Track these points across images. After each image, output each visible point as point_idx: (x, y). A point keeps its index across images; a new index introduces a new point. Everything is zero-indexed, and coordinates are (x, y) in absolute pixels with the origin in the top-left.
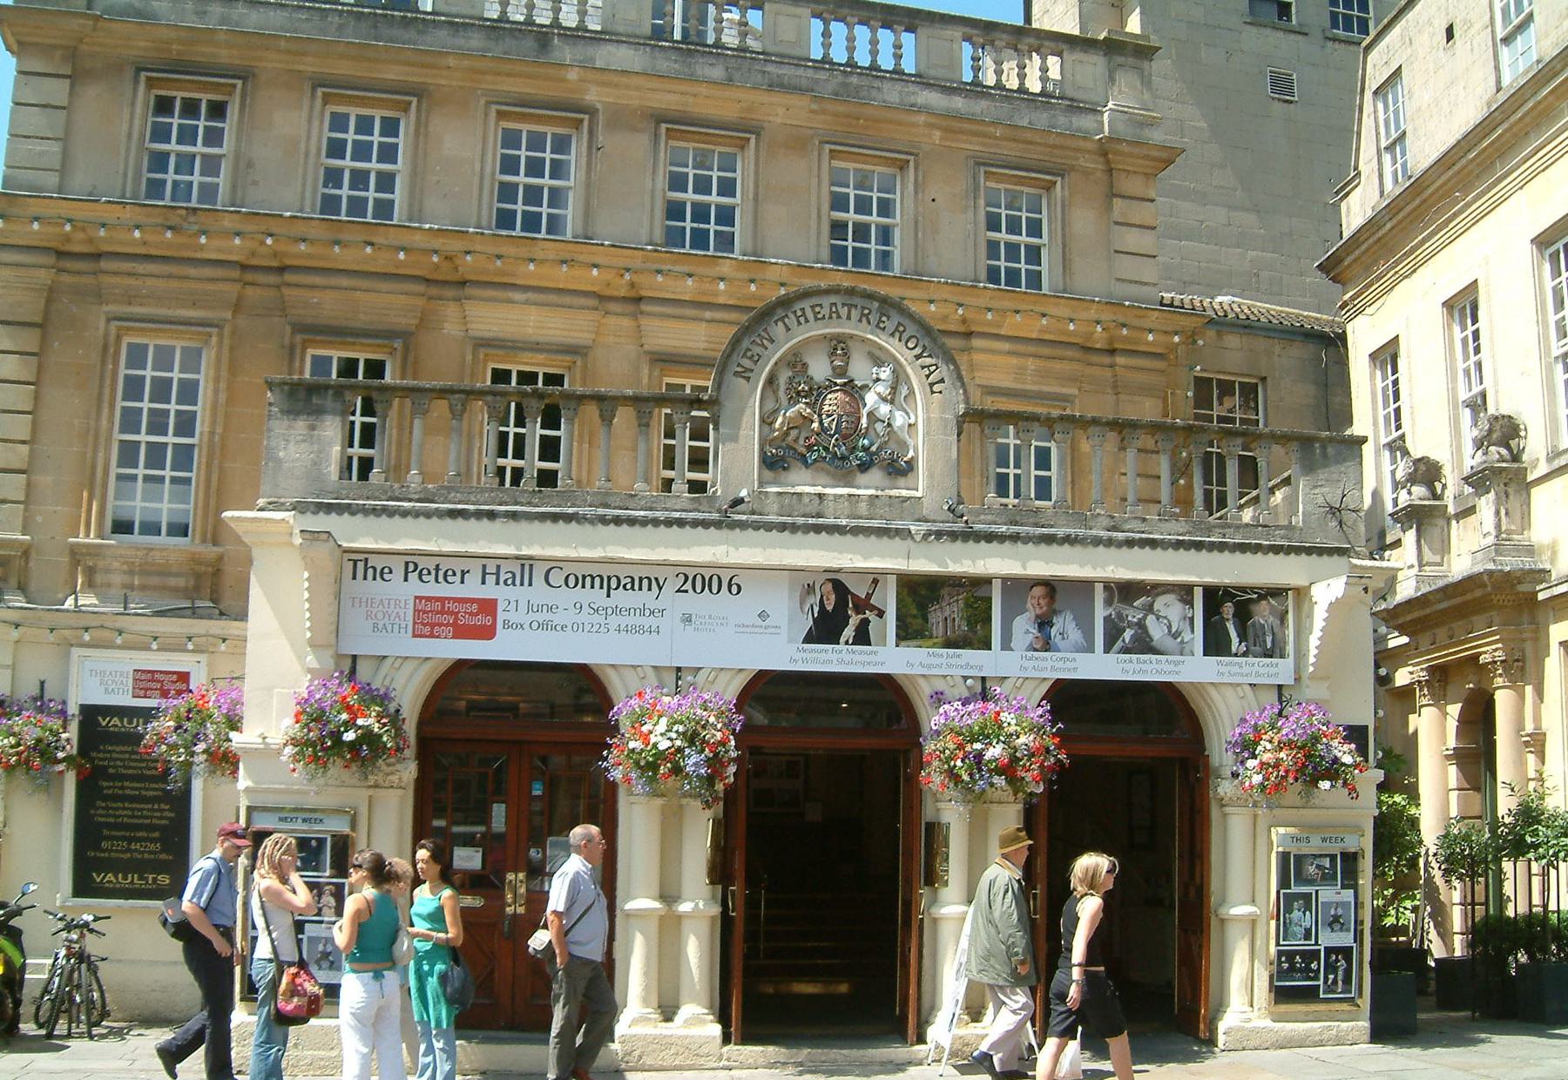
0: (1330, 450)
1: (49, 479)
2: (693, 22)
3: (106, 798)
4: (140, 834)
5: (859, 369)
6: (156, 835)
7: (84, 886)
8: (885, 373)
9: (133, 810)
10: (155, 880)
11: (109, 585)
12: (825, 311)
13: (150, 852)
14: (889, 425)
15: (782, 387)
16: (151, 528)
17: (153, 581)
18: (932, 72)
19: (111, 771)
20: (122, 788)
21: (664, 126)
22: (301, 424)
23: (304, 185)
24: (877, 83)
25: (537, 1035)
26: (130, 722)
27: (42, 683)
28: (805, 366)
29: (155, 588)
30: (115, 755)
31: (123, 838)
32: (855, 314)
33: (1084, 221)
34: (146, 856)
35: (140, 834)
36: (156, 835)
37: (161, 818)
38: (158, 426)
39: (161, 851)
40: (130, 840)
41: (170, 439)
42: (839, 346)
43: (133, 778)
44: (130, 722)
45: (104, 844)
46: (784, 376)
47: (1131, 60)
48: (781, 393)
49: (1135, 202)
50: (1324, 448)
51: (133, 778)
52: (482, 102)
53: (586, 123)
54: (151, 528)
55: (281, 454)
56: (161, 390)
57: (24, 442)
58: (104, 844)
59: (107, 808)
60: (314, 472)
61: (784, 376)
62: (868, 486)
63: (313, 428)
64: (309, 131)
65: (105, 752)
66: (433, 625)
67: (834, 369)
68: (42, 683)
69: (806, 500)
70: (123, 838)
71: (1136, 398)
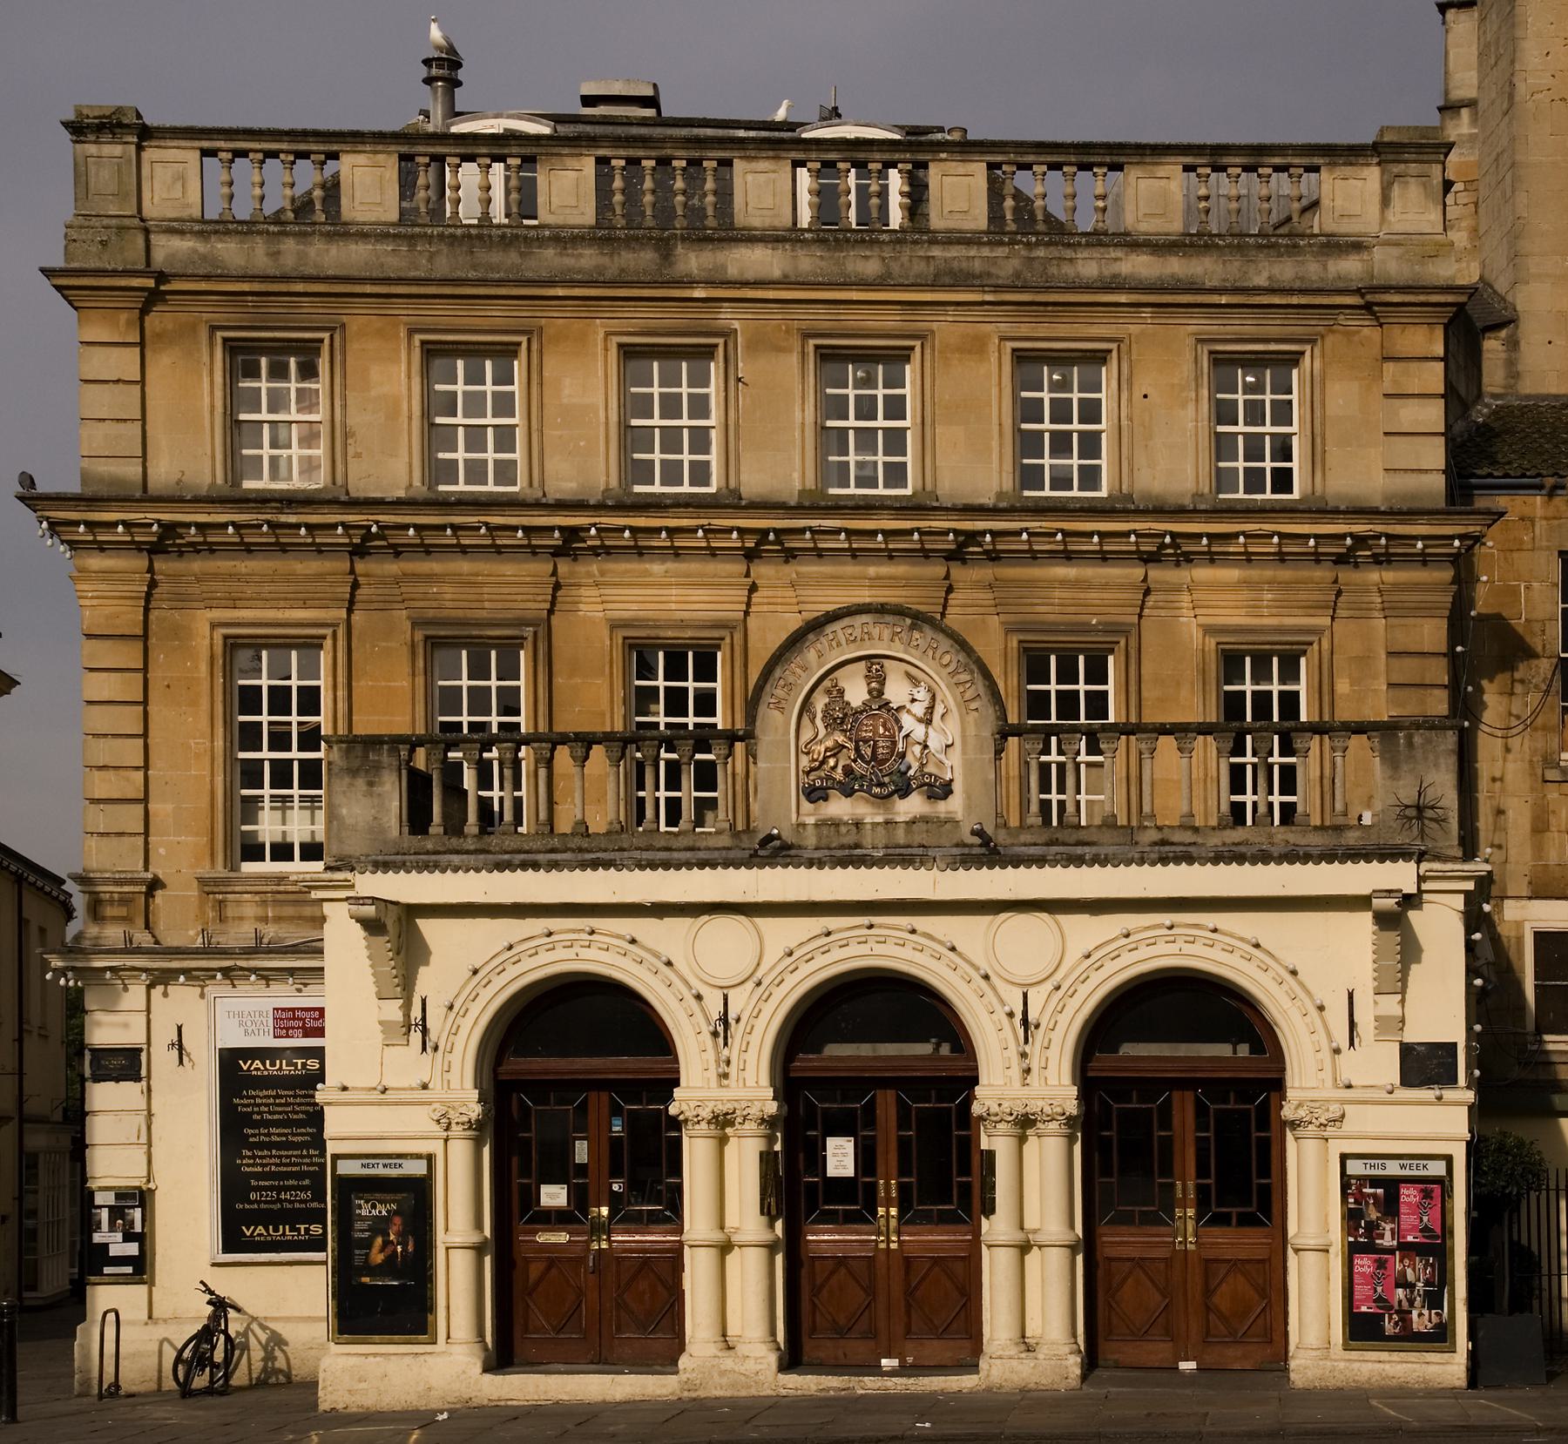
0: (1417, 740)
1: (169, 807)
2: (874, 188)
3: (252, 1147)
4: (291, 1182)
5: (896, 691)
6: (307, 1182)
7: (233, 1240)
8: (922, 694)
9: (280, 1157)
10: (307, 1230)
11: (241, 918)
12: (857, 633)
13: (301, 1202)
14: (926, 747)
15: (819, 715)
16: (282, 851)
17: (289, 911)
18: (1144, 227)
19: (255, 1117)
20: (268, 1135)
21: (812, 342)
22: (360, 783)
23: (410, 453)
24: (1069, 253)
25: (669, 1369)
26: (272, 1064)
27: (180, 1029)
28: (841, 692)
29: (291, 919)
30: (258, 1101)
31: (271, 1188)
32: (887, 633)
33: (1343, 397)
34: (297, 1205)
35: (291, 1182)
36: (307, 1182)
37: (311, 1164)
38: (280, 740)
39: (312, 1200)
40: (279, 1189)
41: (295, 754)
42: (875, 669)
43: (277, 1124)
44: (272, 1064)
45: (253, 1196)
46: (820, 701)
47: (1413, 168)
48: (819, 722)
49: (1414, 365)
50: (1409, 739)
51: (277, 1124)
52: (601, 335)
53: (721, 349)
54: (282, 851)
55: (344, 811)
56: (280, 699)
57: (137, 768)
58: (253, 1196)
59: (254, 1157)
60: (376, 830)
61: (820, 701)
62: (912, 806)
63: (371, 784)
64: (410, 389)
65: (248, 1097)
66: (287, 1029)
67: (870, 692)
68: (180, 1029)
69: (843, 829)
70: (271, 1188)
71: (1412, 621)
